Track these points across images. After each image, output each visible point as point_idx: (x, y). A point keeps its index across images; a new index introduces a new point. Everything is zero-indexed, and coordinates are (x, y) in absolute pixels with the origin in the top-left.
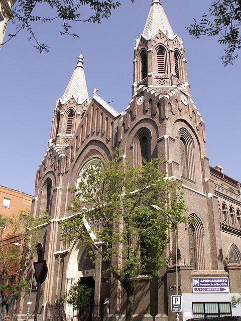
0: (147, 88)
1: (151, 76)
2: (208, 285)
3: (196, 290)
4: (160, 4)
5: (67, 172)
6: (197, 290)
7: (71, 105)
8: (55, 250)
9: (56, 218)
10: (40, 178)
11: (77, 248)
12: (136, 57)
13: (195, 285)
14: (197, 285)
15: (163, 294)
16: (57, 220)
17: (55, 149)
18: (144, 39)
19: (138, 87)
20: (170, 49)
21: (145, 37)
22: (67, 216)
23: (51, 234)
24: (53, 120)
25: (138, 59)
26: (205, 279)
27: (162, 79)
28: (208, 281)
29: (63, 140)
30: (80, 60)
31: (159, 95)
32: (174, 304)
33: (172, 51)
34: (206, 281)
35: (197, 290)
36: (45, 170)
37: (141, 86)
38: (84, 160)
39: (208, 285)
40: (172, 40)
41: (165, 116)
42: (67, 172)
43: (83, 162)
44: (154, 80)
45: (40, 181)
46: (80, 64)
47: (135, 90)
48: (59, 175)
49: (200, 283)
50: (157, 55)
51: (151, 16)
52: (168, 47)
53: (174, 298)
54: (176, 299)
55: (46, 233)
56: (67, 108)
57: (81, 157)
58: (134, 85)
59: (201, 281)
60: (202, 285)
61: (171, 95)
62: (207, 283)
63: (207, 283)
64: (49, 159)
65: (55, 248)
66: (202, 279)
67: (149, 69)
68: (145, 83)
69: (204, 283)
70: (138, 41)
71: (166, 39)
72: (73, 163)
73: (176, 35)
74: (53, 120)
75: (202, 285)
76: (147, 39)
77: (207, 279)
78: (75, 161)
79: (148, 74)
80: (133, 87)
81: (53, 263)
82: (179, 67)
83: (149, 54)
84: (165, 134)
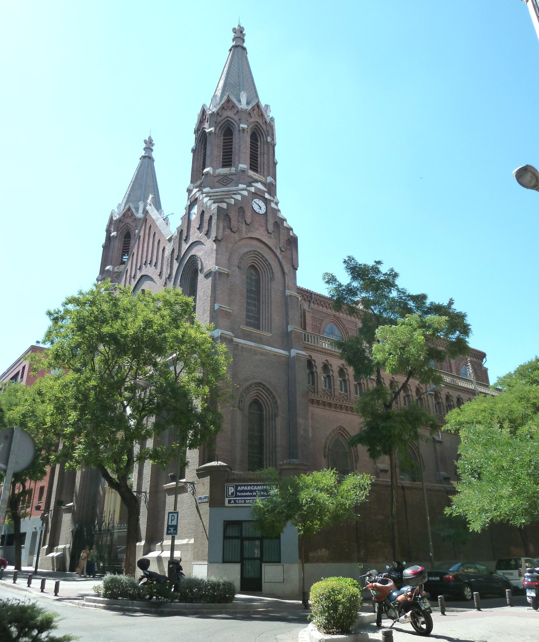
2: (248, 494)
3: (229, 502)
6: (232, 502)
13: (230, 494)
14: (232, 494)
15: (167, 518)
26: (244, 486)
28: (249, 488)
34: (246, 488)
35: (232, 502)
39: (248, 494)
49: (236, 491)
53: (170, 515)
54: (173, 519)
55: (201, 519)
59: (239, 488)
60: (240, 494)
61: (232, 202)
62: (246, 491)
63: (246, 491)
66: (241, 486)
69: (243, 491)
75: (240, 494)
77: (247, 486)
82: (259, 153)
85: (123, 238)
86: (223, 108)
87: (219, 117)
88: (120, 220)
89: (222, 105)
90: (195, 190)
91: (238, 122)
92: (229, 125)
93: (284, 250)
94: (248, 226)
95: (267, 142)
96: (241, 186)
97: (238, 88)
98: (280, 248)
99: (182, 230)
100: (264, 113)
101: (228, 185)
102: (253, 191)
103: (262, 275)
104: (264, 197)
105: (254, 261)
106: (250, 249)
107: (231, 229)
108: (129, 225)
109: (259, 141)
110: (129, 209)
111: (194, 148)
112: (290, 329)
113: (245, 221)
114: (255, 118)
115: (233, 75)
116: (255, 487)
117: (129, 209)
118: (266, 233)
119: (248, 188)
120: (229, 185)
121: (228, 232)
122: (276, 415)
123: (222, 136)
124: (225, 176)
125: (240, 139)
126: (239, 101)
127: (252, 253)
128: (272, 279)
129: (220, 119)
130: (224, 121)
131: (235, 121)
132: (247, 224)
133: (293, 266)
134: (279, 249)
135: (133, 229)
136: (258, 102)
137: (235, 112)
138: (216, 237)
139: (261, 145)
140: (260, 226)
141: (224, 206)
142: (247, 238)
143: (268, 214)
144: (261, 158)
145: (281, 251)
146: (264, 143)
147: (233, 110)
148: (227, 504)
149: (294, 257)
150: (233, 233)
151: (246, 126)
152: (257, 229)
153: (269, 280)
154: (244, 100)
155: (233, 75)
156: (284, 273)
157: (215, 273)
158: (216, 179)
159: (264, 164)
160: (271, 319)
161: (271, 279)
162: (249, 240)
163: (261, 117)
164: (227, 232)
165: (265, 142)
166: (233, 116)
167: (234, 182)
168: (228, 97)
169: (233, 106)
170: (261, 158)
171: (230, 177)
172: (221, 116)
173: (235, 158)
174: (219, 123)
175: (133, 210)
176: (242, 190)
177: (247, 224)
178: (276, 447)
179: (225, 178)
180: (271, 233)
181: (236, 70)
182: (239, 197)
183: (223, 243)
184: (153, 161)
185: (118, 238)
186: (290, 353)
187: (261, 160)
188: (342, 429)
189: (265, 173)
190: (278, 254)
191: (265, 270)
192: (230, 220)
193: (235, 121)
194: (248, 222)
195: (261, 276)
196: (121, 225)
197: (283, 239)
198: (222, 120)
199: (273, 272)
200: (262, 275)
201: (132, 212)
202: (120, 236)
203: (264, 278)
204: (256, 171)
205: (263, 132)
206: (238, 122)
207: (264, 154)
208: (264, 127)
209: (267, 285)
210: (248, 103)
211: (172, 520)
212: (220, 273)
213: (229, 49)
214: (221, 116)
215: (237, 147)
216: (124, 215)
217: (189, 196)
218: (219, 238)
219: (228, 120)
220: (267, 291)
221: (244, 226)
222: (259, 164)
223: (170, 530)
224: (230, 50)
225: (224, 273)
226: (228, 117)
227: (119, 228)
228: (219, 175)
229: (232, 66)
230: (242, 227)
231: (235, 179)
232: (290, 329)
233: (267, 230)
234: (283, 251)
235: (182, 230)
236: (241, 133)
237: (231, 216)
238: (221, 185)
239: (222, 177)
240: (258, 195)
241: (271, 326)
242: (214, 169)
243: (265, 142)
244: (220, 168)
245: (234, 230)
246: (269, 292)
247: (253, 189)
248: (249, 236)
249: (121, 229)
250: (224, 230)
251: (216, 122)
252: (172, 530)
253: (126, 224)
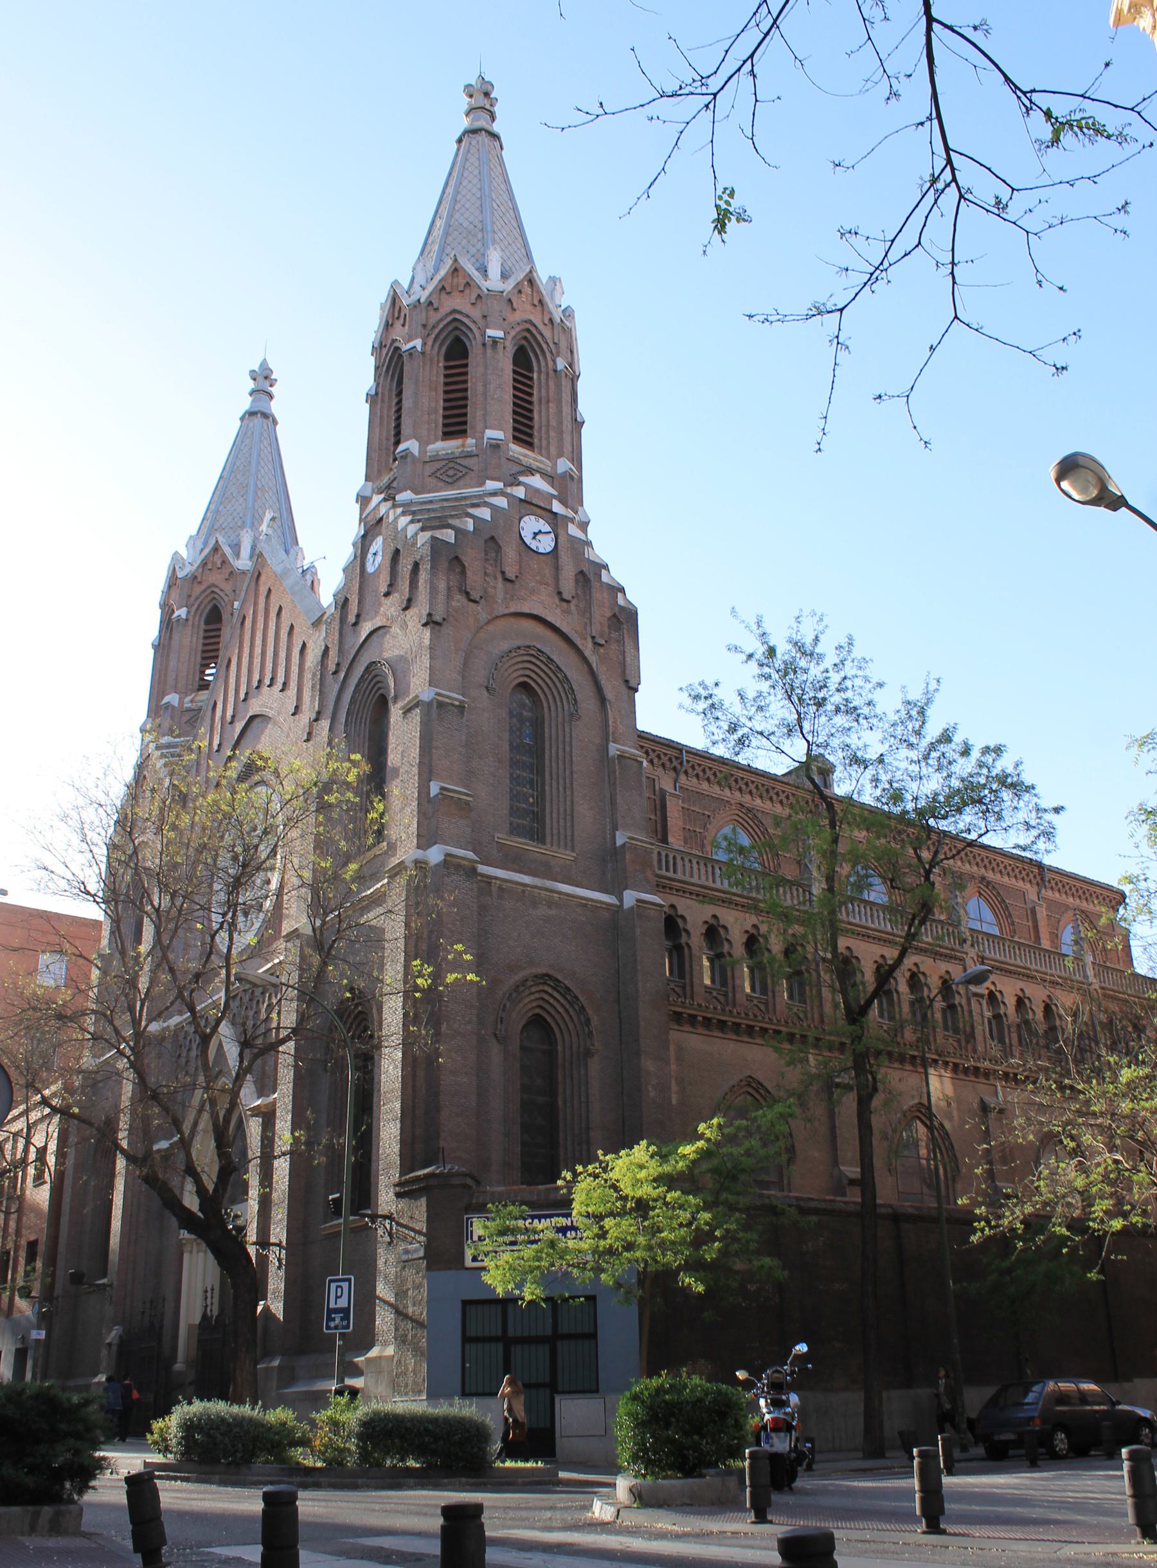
32: (332, 1305)
53: (333, 1286)
85: (202, 623)
86: (443, 288)
87: (432, 313)
88: (194, 578)
89: (440, 281)
90: (377, 499)
91: (481, 322)
92: (457, 333)
93: (603, 642)
94: (509, 585)
95: (555, 371)
96: (491, 485)
97: (480, 236)
98: (593, 638)
99: (346, 600)
100: (547, 299)
101: (457, 484)
102: (523, 497)
103: (549, 707)
104: (551, 511)
105: (527, 672)
106: (518, 643)
107: (467, 594)
108: (216, 590)
109: (535, 368)
110: (216, 549)
111: (373, 392)
112: (620, 840)
113: (503, 573)
114: (525, 311)
115: (467, 206)
116: (536, 1221)
117: (216, 549)
118: (557, 600)
119: (509, 490)
120: (461, 482)
121: (459, 600)
122: (588, 1053)
123: (442, 359)
124: (451, 459)
125: (486, 367)
126: (484, 271)
127: (522, 652)
128: (574, 716)
129: (434, 317)
130: (445, 322)
131: (474, 322)
132: (506, 580)
133: (627, 682)
134: (589, 640)
135: (226, 599)
136: (531, 272)
137: (474, 297)
138: (430, 615)
139: (539, 379)
140: (541, 583)
141: (449, 535)
142: (504, 615)
143: (562, 552)
144: (540, 412)
145: (596, 644)
146: (548, 374)
147: (467, 291)
148: (469, 1263)
149: (628, 659)
150: (471, 604)
151: (499, 334)
152: (533, 592)
153: (567, 718)
154: (494, 270)
155: (467, 206)
156: (602, 700)
157: (430, 704)
158: (429, 469)
159: (548, 426)
160: (572, 817)
161: (571, 715)
162: (512, 620)
163: (539, 308)
164: (458, 601)
165: (551, 373)
166: (467, 309)
167: (472, 474)
168: (456, 260)
169: (468, 284)
170: (540, 412)
171: (463, 462)
172: (436, 309)
173: (474, 413)
174: (434, 327)
175: (227, 550)
176: (494, 494)
177: (506, 580)
178: (588, 1129)
179: (451, 465)
180: (568, 602)
181: (474, 190)
182: (485, 513)
183: (447, 630)
184: (275, 422)
185: (190, 623)
186: (621, 900)
187: (540, 417)
188: (754, 1085)
189: (553, 450)
190: (588, 652)
191: (550, 697)
192: (463, 572)
193: (474, 322)
194: (511, 575)
195: (546, 710)
196: (198, 590)
197: (601, 614)
198: (441, 320)
199: (575, 700)
200: (549, 707)
201: (224, 555)
202: (194, 617)
203: (553, 714)
204: (529, 445)
205: (544, 346)
206: (481, 322)
207: (548, 401)
208: (547, 332)
209: (560, 732)
210: (504, 276)
211: (337, 1297)
212: (441, 705)
213: (457, 136)
214: (436, 309)
215: (480, 388)
216: (204, 564)
217: (361, 514)
218: (438, 618)
219: (455, 320)
220: (561, 746)
221: (500, 584)
222: (536, 427)
223: (334, 1320)
224: (460, 141)
225: (452, 705)
226: (455, 311)
227: (192, 599)
228: (435, 459)
229: (465, 183)
230: (495, 588)
231: (475, 468)
232: (620, 840)
233: (560, 593)
234: (602, 645)
235: (346, 600)
236: (489, 351)
237: (466, 560)
238: (441, 484)
239: (444, 463)
240: (531, 505)
241: (573, 835)
242: (423, 444)
243: (551, 373)
244: (436, 440)
245: (475, 595)
246: (568, 749)
247: (520, 492)
248: (512, 610)
250: (449, 597)
251: (424, 326)
252: (337, 1321)
253: (209, 587)
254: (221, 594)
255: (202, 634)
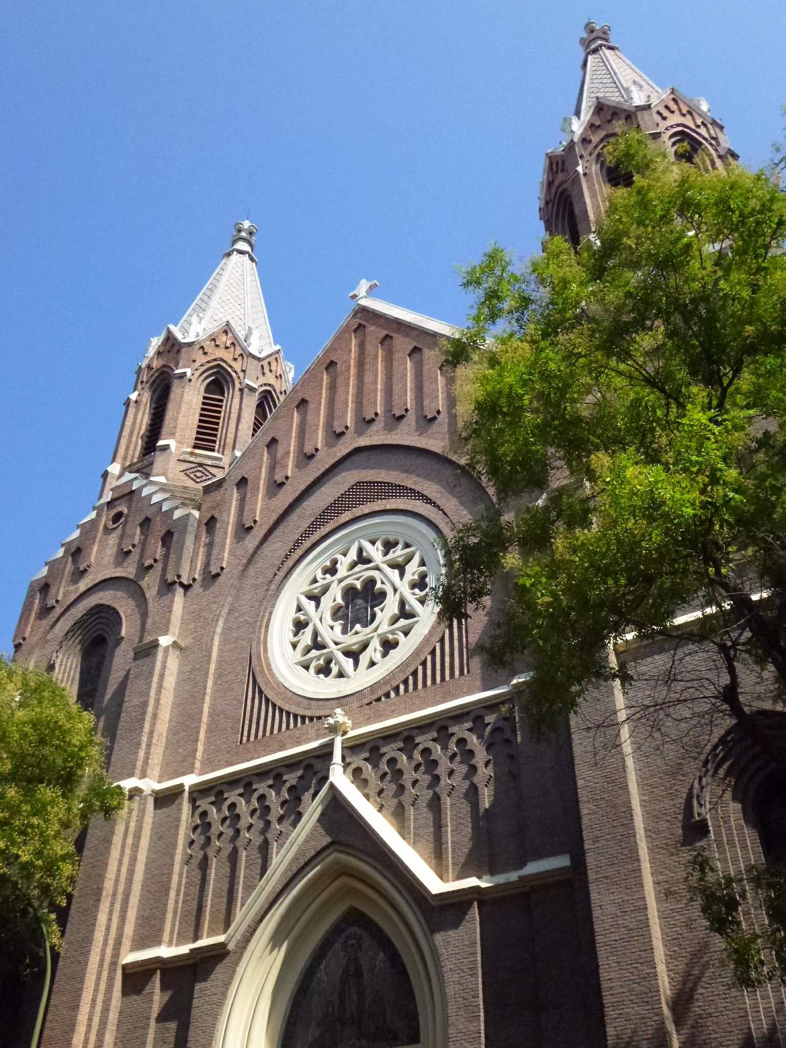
0: (145, 482)
1: (166, 448)
4: (252, 259)
5: (211, 578)
7: (220, 353)
8: (126, 943)
9: (143, 775)
10: (46, 611)
11: (276, 940)
12: (140, 387)
16: (150, 785)
17: (145, 492)
18: (175, 339)
19: (121, 475)
20: (247, 381)
21: (179, 336)
22: (209, 765)
23: (115, 853)
24: (134, 396)
25: (142, 396)
27: (201, 465)
29: (185, 466)
30: (243, 234)
31: (177, 508)
33: (252, 390)
36: (80, 574)
37: (128, 476)
38: (314, 526)
40: (259, 359)
41: (179, 576)
42: (211, 578)
43: (306, 534)
44: (173, 462)
45: (46, 623)
46: (242, 246)
47: (112, 483)
48: (168, 587)
50: (202, 393)
51: (209, 293)
52: (241, 375)
56: (201, 359)
57: (293, 517)
58: (109, 469)
64: (107, 531)
65: (129, 929)
67: (165, 430)
68: (143, 468)
70: (156, 342)
71: (239, 351)
72: (251, 542)
73: (278, 347)
74: (134, 396)
76: (183, 341)
78: (258, 533)
79: (161, 443)
80: (105, 475)
81: (113, 1016)
83: (176, 383)
84: (166, 633)
249: (202, 365)
254: (229, 369)
255: (201, 400)
